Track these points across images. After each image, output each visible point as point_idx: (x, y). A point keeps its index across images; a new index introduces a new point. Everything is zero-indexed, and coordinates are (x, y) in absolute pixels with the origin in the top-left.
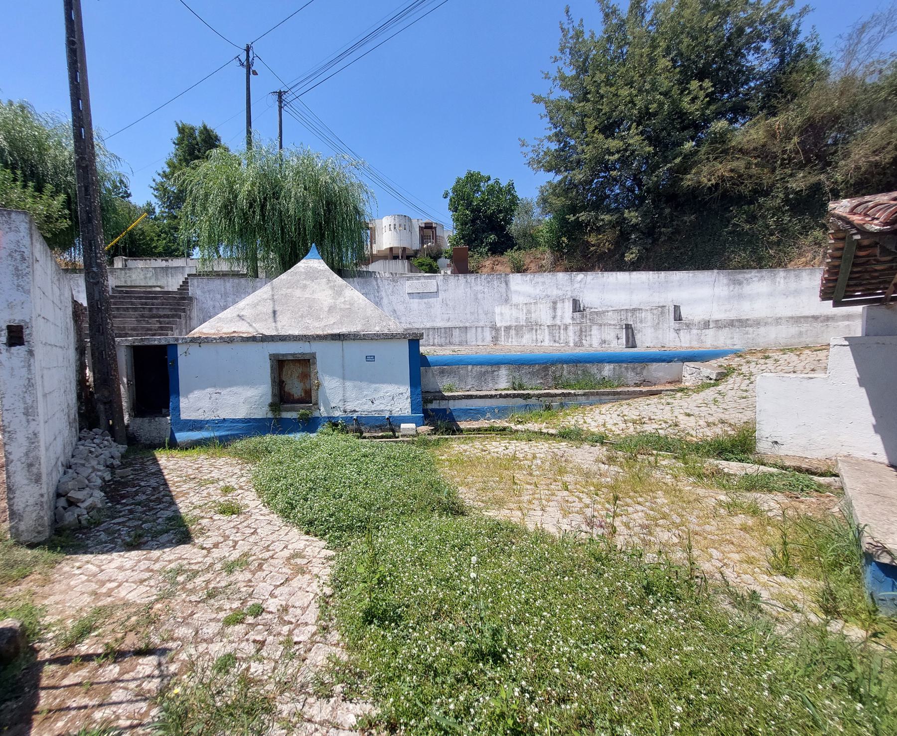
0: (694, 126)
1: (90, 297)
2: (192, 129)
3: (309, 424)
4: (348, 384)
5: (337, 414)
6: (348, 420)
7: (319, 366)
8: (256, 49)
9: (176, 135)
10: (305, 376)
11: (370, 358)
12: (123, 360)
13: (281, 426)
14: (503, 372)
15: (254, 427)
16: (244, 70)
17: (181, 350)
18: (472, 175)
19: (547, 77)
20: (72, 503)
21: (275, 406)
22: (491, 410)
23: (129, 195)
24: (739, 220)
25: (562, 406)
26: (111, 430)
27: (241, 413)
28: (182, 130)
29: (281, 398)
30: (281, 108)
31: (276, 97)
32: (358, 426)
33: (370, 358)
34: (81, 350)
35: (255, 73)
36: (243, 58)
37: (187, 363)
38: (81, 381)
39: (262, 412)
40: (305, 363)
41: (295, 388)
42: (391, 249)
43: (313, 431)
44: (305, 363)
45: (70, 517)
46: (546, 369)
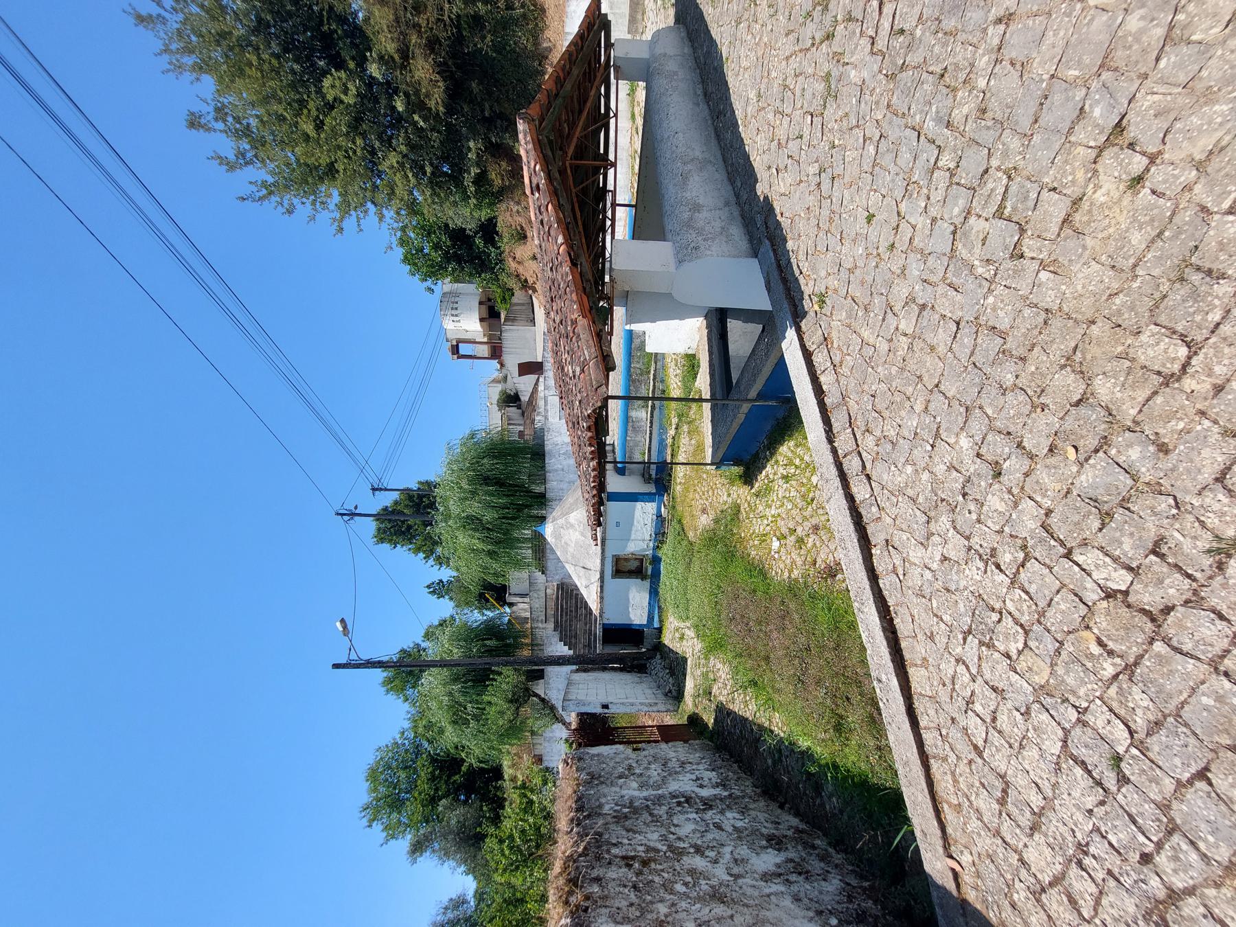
0: (372, 93)
1: (574, 664)
2: (379, 529)
3: (656, 561)
4: (633, 537)
5: (651, 545)
6: (656, 540)
7: (621, 553)
8: (337, 507)
9: (386, 546)
10: (626, 560)
11: (618, 524)
12: (611, 650)
13: (655, 577)
14: (633, 414)
15: (654, 592)
16: (356, 518)
17: (606, 622)
18: (406, 258)
19: (313, 218)
20: (670, 691)
21: (643, 578)
22: (660, 434)
23: (441, 581)
24: (485, 43)
25: (662, 381)
26: (648, 659)
27: (646, 597)
28: (382, 540)
29: (638, 573)
30: (386, 490)
31: (377, 493)
32: (660, 535)
33: (618, 524)
34: (604, 669)
35: (356, 508)
36: (346, 518)
37: (614, 618)
38: (621, 670)
39: (647, 583)
40: (617, 560)
41: (633, 565)
42: (481, 320)
43: (660, 559)
44: (617, 560)
45: (674, 693)
46: (634, 381)
